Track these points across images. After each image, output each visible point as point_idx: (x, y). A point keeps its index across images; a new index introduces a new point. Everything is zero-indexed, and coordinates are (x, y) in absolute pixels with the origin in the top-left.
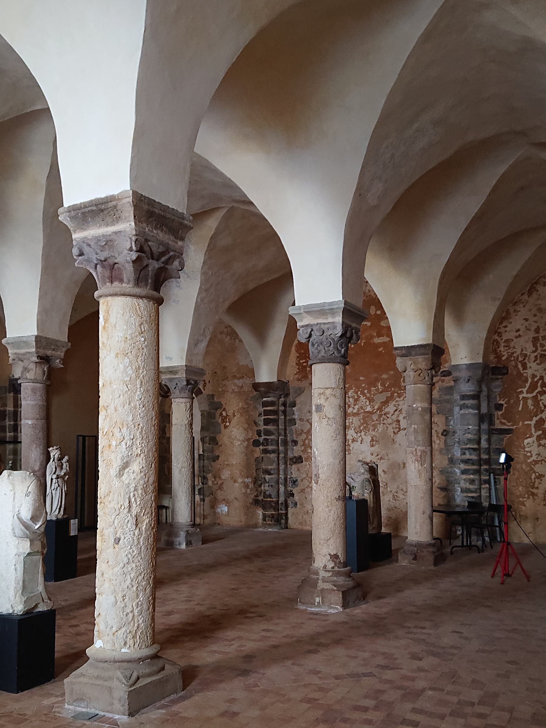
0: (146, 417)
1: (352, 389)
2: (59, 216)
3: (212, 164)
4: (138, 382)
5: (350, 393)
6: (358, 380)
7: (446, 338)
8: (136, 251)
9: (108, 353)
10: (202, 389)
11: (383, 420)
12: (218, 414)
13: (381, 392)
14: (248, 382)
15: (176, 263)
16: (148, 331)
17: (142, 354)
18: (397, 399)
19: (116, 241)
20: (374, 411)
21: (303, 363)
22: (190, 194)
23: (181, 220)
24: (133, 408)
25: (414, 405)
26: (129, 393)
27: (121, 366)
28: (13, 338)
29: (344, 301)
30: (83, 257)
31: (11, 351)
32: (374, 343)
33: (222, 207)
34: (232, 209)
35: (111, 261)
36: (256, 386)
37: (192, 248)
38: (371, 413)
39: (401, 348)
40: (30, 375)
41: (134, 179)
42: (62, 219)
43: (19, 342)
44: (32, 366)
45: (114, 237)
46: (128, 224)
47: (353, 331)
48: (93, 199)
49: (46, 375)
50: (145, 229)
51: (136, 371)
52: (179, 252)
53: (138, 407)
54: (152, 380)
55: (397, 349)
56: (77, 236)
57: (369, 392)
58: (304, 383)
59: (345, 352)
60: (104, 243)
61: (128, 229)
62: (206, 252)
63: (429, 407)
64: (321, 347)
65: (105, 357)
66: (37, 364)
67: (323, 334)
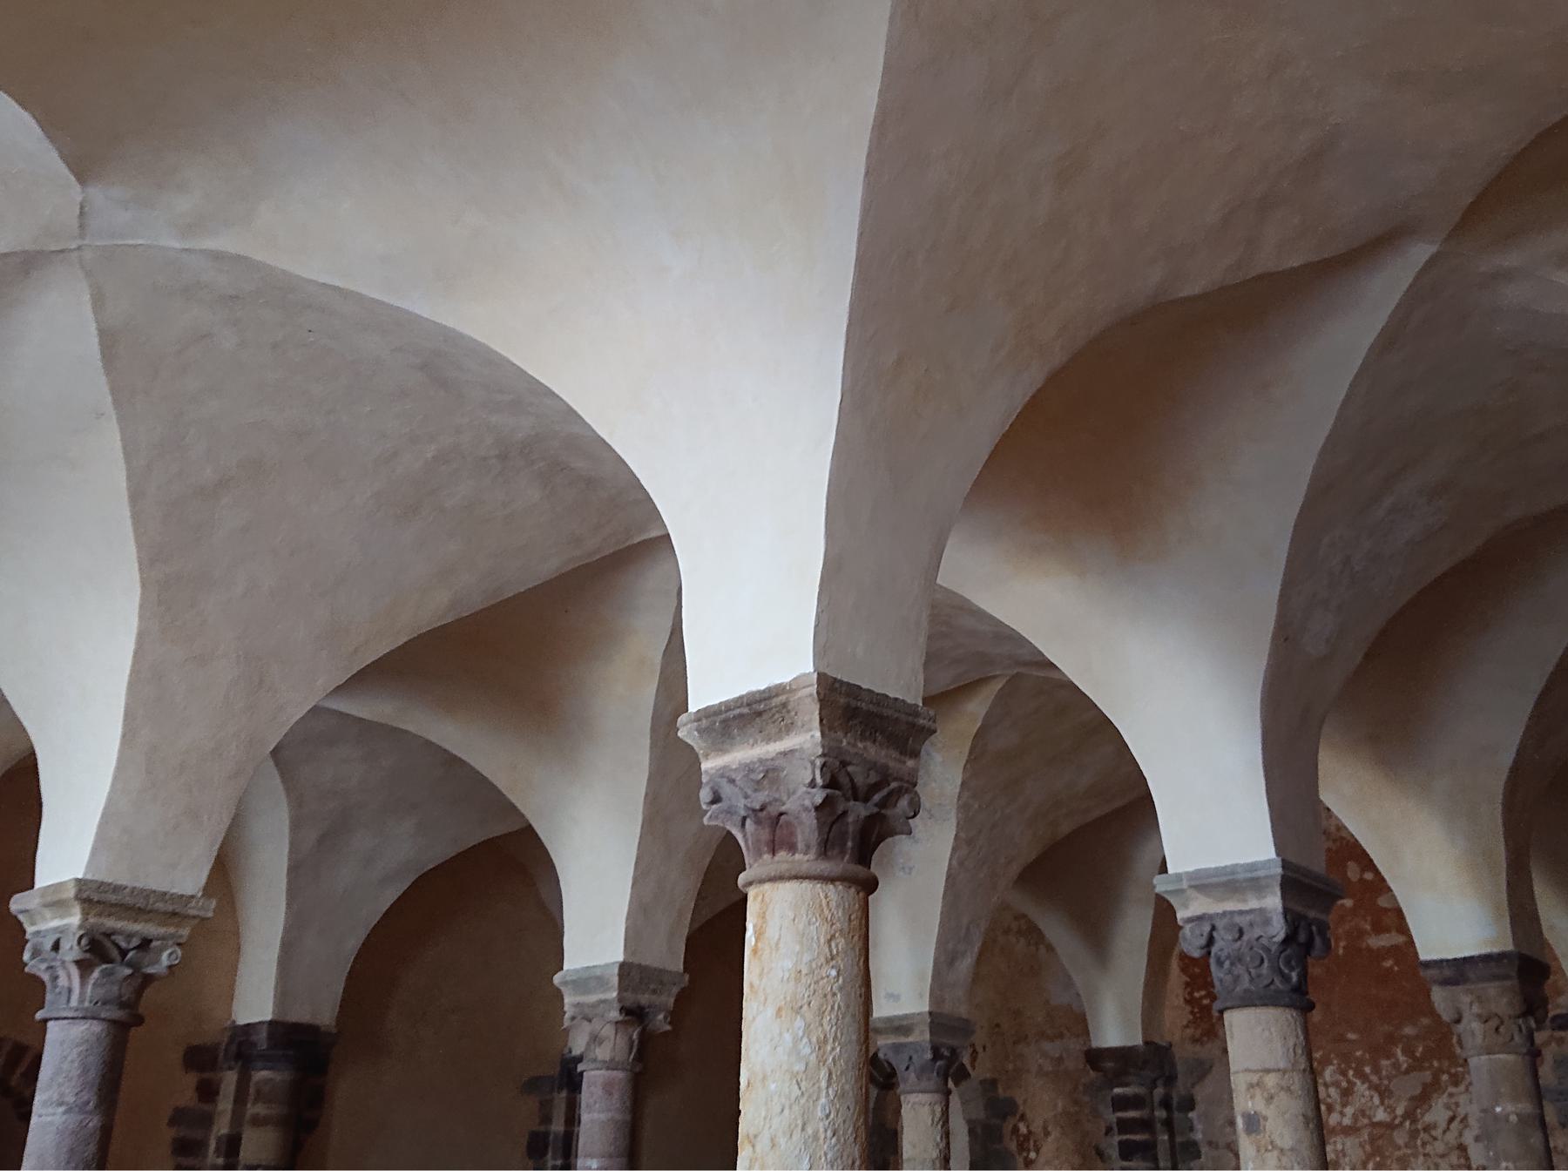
0: (839, 1160)
1: (1331, 1064)
2: (678, 730)
3: (972, 603)
4: (823, 1074)
5: (1329, 1074)
6: (1341, 1039)
7: (1547, 934)
8: (824, 787)
9: (761, 1008)
10: (969, 1067)
11: (1424, 1144)
12: (1007, 1127)
13: (1407, 1072)
14: (1075, 1046)
15: (903, 803)
16: (845, 952)
17: (833, 1008)
18: (1451, 1089)
19: (783, 770)
20: (1397, 1122)
21: (1202, 998)
22: (931, 660)
23: (910, 719)
24: (811, 1140)
25: (1498, 1109)
26: (803, 1101)
27: (788, 1037)
28: (576, 971)
29: (1280, 859)
30: (720, 805)
31: (568, 1000)
32: (1369, 949)
33: (994, 677)
34: (1014, 680)
35: (773, 810)
36: (1095, 1057)
37: (938, 758)
38: (1390, 1126)
39: (1439, 964)
40: (603, 1053)
41: (820, 650)
42: (684, 736)
43: (587, 981)
44: (608, 1031)
45: (779, 762)
46: (808, 736)
47: (1314, 928)
48: (744, 693)
49: (634, 1050)
50: (841, 742)
51: (819, 1049)
52: (908, 782)
53: (823, 1137)
54: (853, 1068)
55: (1428, 965)
56: (710, 765)
57: (1377, 1070)
58: (1207, 1051)
59: (1299, 981)
60: (762, 775)
61: (807, 746)
62: (965, 766)
63: (1538, 1111)
64: (1240, 969)
65: (754, 1018)
66: (619, 1025)
67: (1240, 937)
